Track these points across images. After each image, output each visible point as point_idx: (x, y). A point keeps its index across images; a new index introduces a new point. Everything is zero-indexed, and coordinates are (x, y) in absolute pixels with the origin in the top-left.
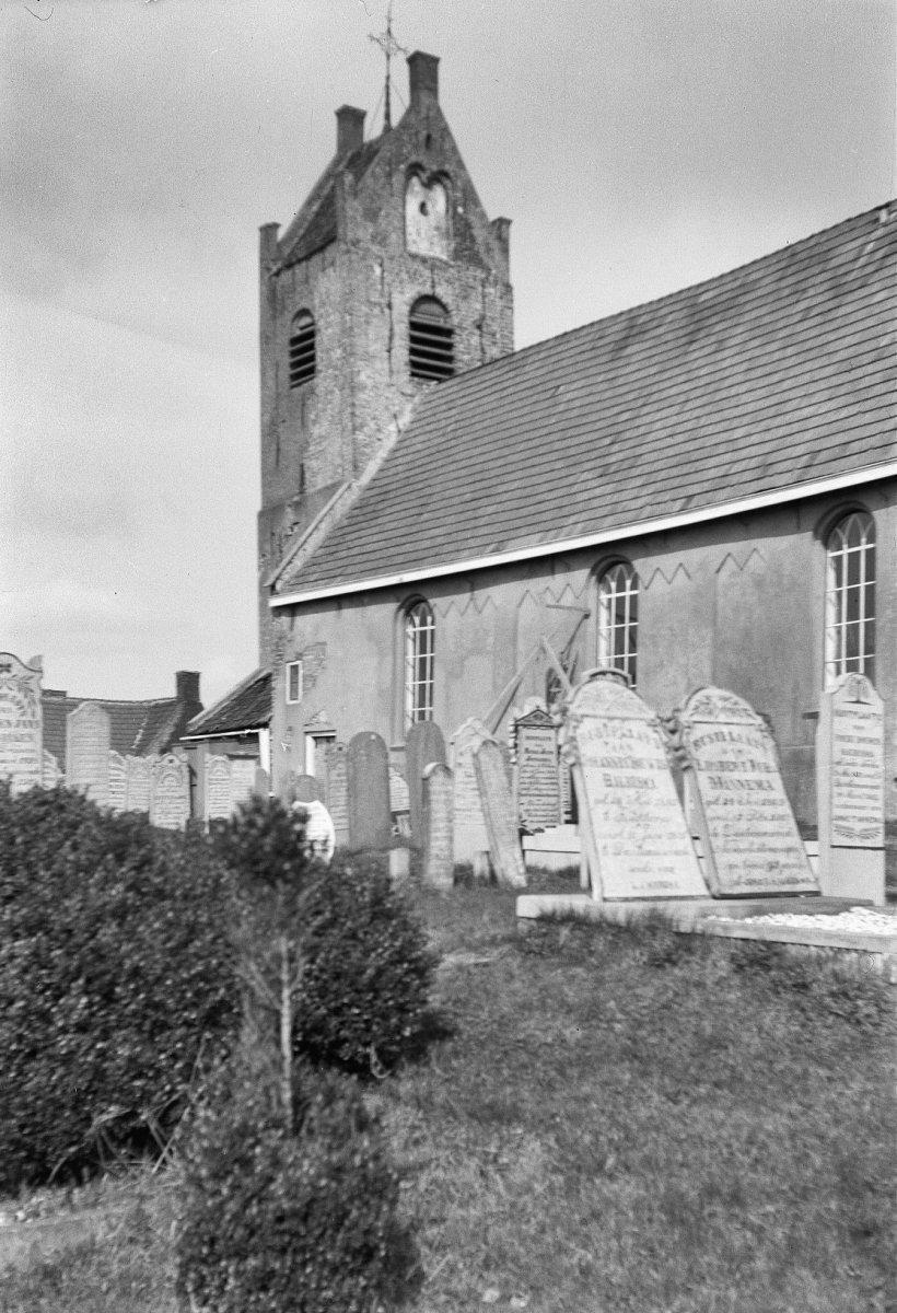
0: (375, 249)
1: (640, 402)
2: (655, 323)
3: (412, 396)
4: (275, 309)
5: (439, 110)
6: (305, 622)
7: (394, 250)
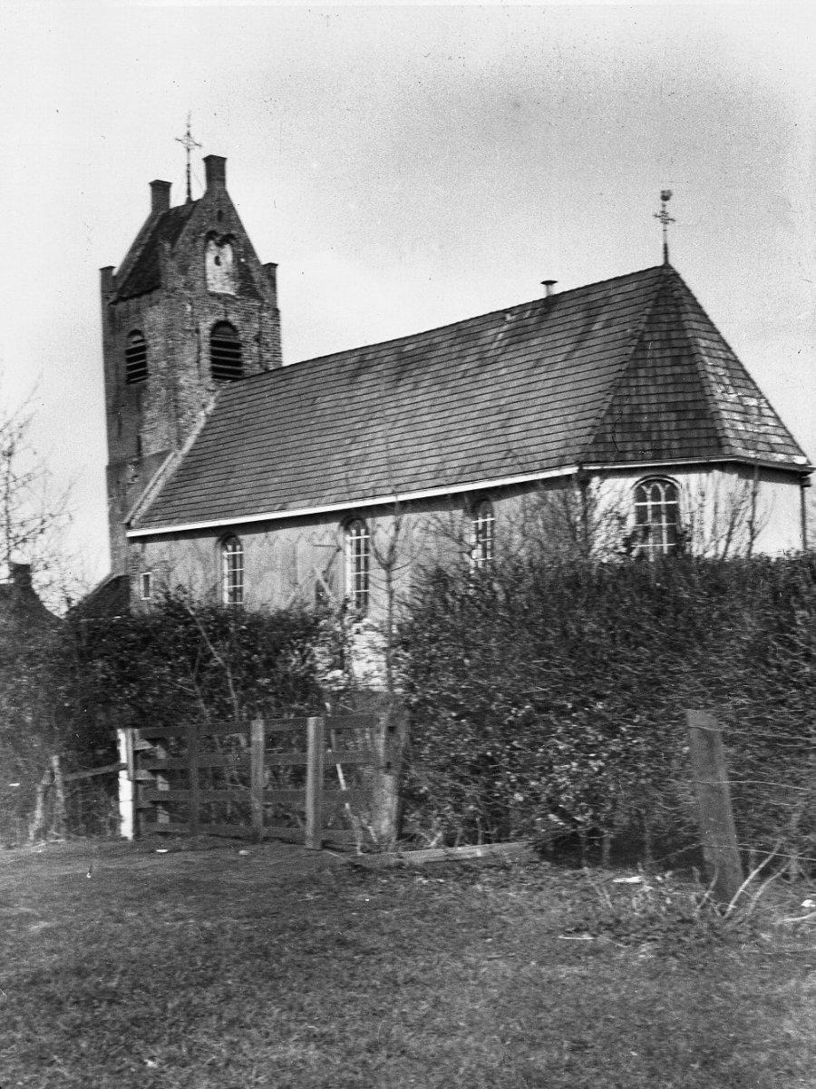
0: (187, 293)
1: (368, 417)
2: (376, 362)
4: (113, 326)
5: (226, 193)
6: (154, 549)
7: (199, 292)
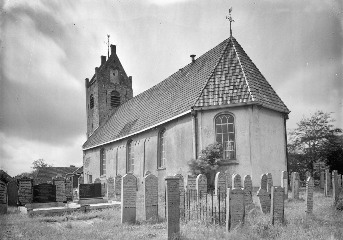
3: (111, 110)
